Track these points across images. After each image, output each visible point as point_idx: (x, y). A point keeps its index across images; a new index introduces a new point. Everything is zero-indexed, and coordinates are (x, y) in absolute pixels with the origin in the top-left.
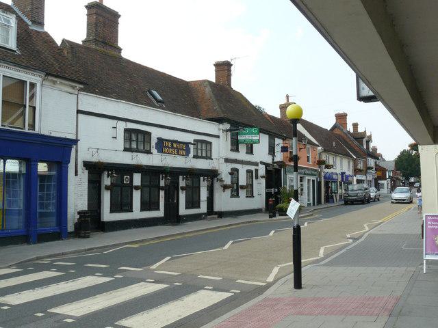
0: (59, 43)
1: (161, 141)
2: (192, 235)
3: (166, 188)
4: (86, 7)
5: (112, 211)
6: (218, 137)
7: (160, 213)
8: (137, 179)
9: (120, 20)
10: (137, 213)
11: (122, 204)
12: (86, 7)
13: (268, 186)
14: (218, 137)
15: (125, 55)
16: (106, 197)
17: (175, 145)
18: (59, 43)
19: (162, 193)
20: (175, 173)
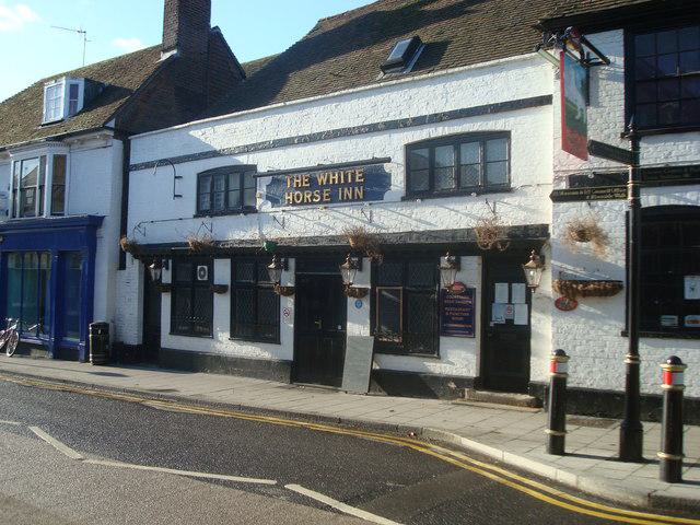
1: (277, 178)
5: (276, 340)
8: (223, 271)
19: (288, 303)
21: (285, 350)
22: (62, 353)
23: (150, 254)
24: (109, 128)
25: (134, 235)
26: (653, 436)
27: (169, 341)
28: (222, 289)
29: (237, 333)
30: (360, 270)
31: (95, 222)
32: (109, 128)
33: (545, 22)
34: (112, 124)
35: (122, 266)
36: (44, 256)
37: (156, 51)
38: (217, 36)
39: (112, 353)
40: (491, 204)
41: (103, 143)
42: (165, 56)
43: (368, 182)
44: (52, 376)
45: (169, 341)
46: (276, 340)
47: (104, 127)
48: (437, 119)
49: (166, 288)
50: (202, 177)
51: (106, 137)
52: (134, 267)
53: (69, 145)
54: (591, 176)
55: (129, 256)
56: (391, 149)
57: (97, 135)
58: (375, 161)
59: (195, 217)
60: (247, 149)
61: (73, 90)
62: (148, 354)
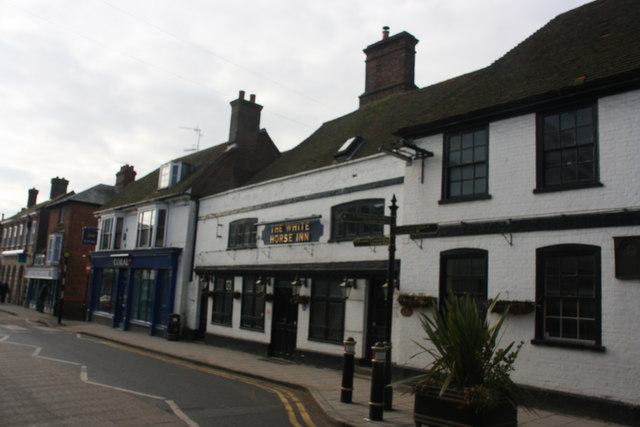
0: (261, 128)
1: (269, 226)
2: (157, 357)
3: (311, 302)
4: (365, 51)
5: (262, 330)
6: (399, 181)
7: (265, 337)
8: (238, 285)
9: (418, 48)
10: (235, 331)
11: (224, 318)
12: (365, 51)
13: (255, 235)
14: (399, 181)
15: (352, 105)
16: (303, 317)
17: (289, 228)
18: (261, 128)
19: (269, 307)
20: (284, 275)
21: (265, 337)
22: (154, 333)
23: (207, 273)
24: (187, 194)
25: (198, 262)
26: (362, 388)
27: (212, 328)
28: (237, 295)
29: (244, 324)
30: (356, 288)
31: (177, 252)
32: (187, 194)
33: (400, 130)
34: (189, 191)
35: (191, 280)
36: (152, 272)
37: (224, 146)
38: (264, 133)
39: (179, 332)
40: (509, 239)
41: (183, 203)
42: (229, 148)
43: (312, 228)
44: (89, 332)
45: (303, 341)
46: (262, 330)
47: (184, 194)
48: (349, 190)
49: (269, 298)
50: (232, 226)
51: (185, 200)
52: (196, 280)
53: (168, 203)
54: (508, 222)
55: (194, 274)
56: (323, 209)
57: (181, 198)
58: (314, 217)
59: (228, 250)
60: (255, 208)
61: (174, 170)
62: (199, 336)
